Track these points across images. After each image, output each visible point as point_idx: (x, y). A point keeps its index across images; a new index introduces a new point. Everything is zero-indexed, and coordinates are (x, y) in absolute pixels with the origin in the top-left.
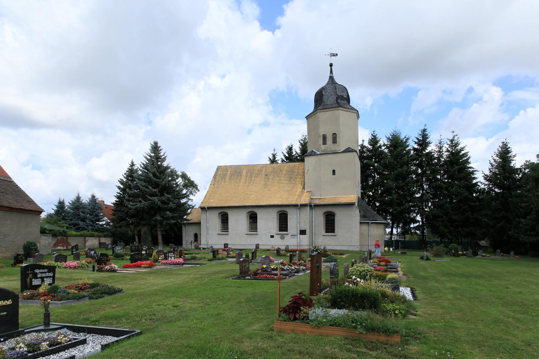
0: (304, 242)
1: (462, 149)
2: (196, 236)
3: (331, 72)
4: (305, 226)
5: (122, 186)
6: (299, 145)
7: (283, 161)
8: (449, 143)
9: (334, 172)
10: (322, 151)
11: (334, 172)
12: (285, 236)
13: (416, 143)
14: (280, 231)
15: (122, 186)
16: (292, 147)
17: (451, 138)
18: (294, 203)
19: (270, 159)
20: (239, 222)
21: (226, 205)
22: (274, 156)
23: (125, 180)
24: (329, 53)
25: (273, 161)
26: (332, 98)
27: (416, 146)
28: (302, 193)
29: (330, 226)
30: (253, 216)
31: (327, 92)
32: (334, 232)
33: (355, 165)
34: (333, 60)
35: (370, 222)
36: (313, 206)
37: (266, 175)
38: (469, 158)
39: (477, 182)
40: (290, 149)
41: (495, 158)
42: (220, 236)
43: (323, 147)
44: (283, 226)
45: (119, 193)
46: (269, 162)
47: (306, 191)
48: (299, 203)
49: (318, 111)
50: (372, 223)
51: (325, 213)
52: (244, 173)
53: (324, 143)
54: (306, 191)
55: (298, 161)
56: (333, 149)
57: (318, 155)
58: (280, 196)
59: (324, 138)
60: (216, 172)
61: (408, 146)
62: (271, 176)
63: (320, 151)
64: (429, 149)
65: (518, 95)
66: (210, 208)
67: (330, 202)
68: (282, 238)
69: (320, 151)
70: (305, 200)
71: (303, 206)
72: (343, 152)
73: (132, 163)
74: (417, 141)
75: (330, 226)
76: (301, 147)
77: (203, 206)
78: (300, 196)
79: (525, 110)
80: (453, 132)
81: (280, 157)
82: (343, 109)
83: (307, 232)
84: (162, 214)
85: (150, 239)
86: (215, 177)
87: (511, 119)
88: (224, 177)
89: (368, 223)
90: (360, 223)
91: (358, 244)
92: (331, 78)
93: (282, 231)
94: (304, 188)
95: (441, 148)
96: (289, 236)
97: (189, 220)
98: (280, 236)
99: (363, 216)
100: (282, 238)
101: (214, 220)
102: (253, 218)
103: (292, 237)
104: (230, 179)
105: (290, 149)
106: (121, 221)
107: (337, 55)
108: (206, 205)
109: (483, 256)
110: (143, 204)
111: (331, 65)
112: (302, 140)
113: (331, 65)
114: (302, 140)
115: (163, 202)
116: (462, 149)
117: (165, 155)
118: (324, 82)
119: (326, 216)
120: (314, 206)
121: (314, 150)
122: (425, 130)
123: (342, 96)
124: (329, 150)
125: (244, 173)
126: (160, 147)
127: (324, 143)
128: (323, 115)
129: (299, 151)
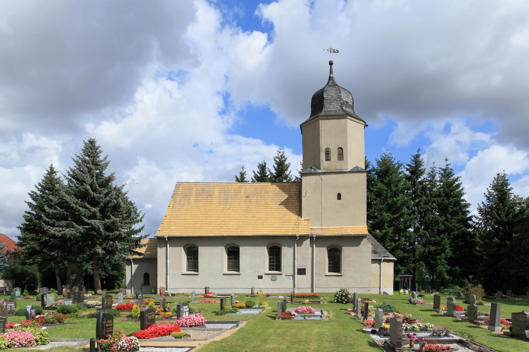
1: (457, 179)
3: (331, 72)
5: (34, 203)
6: (273, 163)
7: (253, 181)
9: (339, 197)
10: (324, 169)
11: (339, 197)
12: (277, 276)
13: (407, 170)
14: (270, 269)
15: (34, 203)
16: (265, 166)
18: (290, 233)
22: (242, 175)
23: (39, 193)
27: (407, 173)
29: (335, 265)
33: (357, 190)
34: (333, 57)
38: (462, 189)
39: (472, 216)
40: (263, 167)
41: (491, 191)
44: (275, 263)
45: (29, 213)
47: (303, 219)
48: (298, 234)
49: (320, 117)
53: (328, 159)
59: (328, 153)
60: (175, 190)
72: (351, 172)
73: (52, 168)
75: (335, 265)
76: (276, 166)
78: (297, 225)
81: (249, 176)
82: (350, 118)
90: (372, 260)
93: (273, 270)
95: (433, 177)
96: (284, 275)
99: (374, 252)
101: (178, 256)
102: (233, 254)
105: (263, 167)
106: (33, 255)
109: (502, 297)
110: (73, 231)
111: (331, 64)
112: (278, 158)
113: (331, 64)
114: (278, 158)
116: (457, 179)
117: (107, 160)
118: (322, 84)
120: (316, 237)
123: (347, 102)
124: (333, 170)
126: (98, 147)
127: (328, 159)
129: (274, 172)
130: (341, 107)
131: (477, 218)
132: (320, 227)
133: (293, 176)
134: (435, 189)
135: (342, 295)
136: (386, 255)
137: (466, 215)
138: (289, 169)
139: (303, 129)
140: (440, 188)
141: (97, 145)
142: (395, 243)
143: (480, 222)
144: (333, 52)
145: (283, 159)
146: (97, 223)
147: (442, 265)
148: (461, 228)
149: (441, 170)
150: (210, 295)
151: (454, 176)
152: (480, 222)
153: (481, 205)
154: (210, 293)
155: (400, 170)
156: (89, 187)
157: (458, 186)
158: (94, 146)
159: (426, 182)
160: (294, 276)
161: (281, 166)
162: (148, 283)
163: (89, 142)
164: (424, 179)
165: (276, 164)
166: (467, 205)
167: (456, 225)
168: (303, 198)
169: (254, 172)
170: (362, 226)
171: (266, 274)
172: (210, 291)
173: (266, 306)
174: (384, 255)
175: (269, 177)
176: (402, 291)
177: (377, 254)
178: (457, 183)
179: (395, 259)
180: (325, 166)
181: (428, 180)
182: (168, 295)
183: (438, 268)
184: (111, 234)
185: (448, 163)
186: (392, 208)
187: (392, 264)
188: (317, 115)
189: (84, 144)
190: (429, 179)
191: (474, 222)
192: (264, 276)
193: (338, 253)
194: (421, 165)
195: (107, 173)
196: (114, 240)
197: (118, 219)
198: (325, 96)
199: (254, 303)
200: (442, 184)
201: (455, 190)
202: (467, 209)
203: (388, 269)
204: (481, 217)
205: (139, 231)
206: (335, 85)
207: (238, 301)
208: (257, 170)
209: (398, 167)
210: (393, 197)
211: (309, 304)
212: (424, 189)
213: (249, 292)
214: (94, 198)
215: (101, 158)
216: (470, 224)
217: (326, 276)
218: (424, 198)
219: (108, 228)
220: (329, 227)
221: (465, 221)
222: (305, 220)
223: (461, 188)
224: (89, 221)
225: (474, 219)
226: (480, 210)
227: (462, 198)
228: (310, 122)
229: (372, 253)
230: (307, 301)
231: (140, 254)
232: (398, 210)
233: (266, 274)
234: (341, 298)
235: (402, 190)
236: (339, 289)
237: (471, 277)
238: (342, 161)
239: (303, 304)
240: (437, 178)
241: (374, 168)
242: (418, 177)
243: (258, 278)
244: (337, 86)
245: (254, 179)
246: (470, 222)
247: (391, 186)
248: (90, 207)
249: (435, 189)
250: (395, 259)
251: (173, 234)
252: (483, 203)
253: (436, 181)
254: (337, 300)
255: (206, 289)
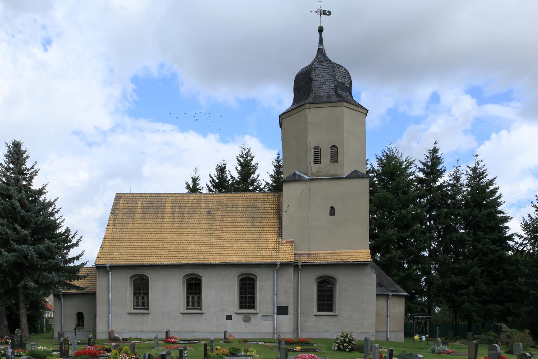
0: (285, 325)
1: (491, 183)
2: (80, 316)
3: (321, 42)
4: (288, 301)
6: (236, 163)
8: (471, 173)
9: (332, 211)
11: (332, 211)
12: (251, 316)
13: (420, 170)
14: (241, 308)
16: (225, 168)
17: (473, 165)
18: (268, 260)
19: (188, 186)
20: (167, 293)
21: (146, 262)
22: (194, 180)
24: (317, 8)
25: (194, 188)
26: (321, 86)
27: (421, 175)
28: (280, 244)
29: (326, 301)
30: (194, 282)
31: (319, 74)
32: (331, 310)
33: (357, 202)
34: (324, 21)
35: (391, 294)
36: (296, 267)
37: (209, 212)
38: (500, 197)
39: (512, 235)
40: (222, 170)
42: (133, 317)
43: (315, 168)
44: (248, 297)
46: (186, 191)
47: (284, 241)
48: (278, 261)
49: (307, 106)
50: (393, 295)
51: (132, 277)
52: (168, 208)
53: (317, 161)
54: (284, 241)
55: (237, 190)
56: (332, 172)
57: (306, 180)
58: (240, 247)
59: (317, 152)
61: (410, 174)
62: (218, 215)
63: (310, 174)
64: (440, 181)
65: (493, 110)
66: (115, 267)
67: (329, 260)
68: (247, 319)
69: (310, 174)
70: (286, 255)
71: (284, 265)
74: (422, 167)
75: (326, 301)
77: (100, 263)
78: (277, 249)
79: (497, 132)
80: (477, 156)
81: (204, 184)
82: (348, 105)
83: (291, 310)
84: (36, 277)
85: (6, 323)
86: (114, 211)
87: (478, 147)
88: (131, 213)
89: (388, 295)
90: (377, 295)
91: (374, 330)
92: (321, 51)
93: (246, 308)
94: (280, 234)
95: (458, 179)
96: (259, 316)
97: (83, 289)
98: (242, 316)
99: (379, 285)
100: (247, 319)
101: (122, 289)
102: (194, 287)
103: (264, 318)
104: (143, 217)
105: (222, 170)
107: (330, 13)
108: (107, 262)
111: (321, 30)
112: (242, 157)
113: (321, 30)
114: (242, 157)
115: (41, 255)
116: (491, 183)
117: (36, 168)
118: (308, 58)
119: (241, 280)
120: (302, 266)
121: (298, 173)
122: (435, 151)
123: (343, 84)
125: (168, 208)
127: (317, 161)
128: (315, 115)
129: (236, 175)
130: (336, 91)
131: (520, 237)
132: (307, 252)
133: (262, 181)
134: (459, 197)
135: (345, 341)
136: (395, 290)
137: (506, 232)
138: (257, 172)
139: (284, 121)
140: (468, 194)
141: (23, 149)
142: (404, 272)
143: (525, 242)
144: (324, 14)
145: (249, 158)
146: (31, 250)
147: (471, 302)
148: (497, 251)
149: (468, 169)
150: (173, 340)
151: (487, 178)
152: (525, 242)
153: (527, 219)
154: (171, 338)
155: (410, 171)
156: (17, 204)
157: (494, 192)
158: (19, 150)
159: (446, 186)
160: (272, 316)
161: (247, 167)
162: (83, 325)
163: (13, 144)
164: (444, 182)
165: (239, 165)
166: (507, 219)
167: (491, 247)
168: (284, 214)
169: (211, 176)
170: (363, 251)
171: (237, 313)
172: (171, 336)
173: (253, 353)
174: (392, 289)
175: (230, 182)
176: (417, 337)
177: (383, 288)
178: (492, 187)
179: (406, 294)
180: (314, 171)
181: (449, 185)
182: (119, 340)
183: (463, 306)
184: (45, 263)
185: (479, 159)
186: (404, 224)
187: (403, 301)
188: (302, 103)
189: (7, 148)
190: (451, 182)
191: (517, 243)
192: (235, 317)
193: (331, 286)
194: (440, 163)
195: (36, 185)
196: (50, 271)
197: (54, 244)
198: (314, 77)
199: (239, 350)
200: (469, 189)
201: (489, 198)
202: (506, 225)
203: (397, 309)
204: (526, 236)
205: (77, 258)
206: (327, 60)
207: (219, 348)
208: (214, 173)
209: (407, 167)
210: (401, 209)
211: (301, 351)
212: (445, 196)
213: (222, 336)
214: (23, 218)
215: (28, 164)
216: (509, 245)
217: (315, 316)
218: (445, 210)
219: (41, 255)
220: (318, 252)
221: (502, 239)
222: (287, 242)
223: (497, 194)
224: (20, 247)
225: (516, 239)
226: (526, 226)
227: (499, 208)
228: (294, 112)
229: (377, 287)
230: (298, 348)
231: (77, 288)
232: (408, 227)
233: (237, 313)
234: (343, 345)
235: (413, 199)
236: (340, 334)
237: (510, 319)
238: (336, 164)
239: (293, 351)
240: (464, 180)
241: (373, 168)
242: (435, 180)
243: (227, 319)
244: (330, 61)
245: (210, 184)
246: (511, 243)
247: (397, 194)
248: (21, 230)
249: (459, 197)
250: (406, 294)
251: (116, 262)
252: (529, 216)
253: (462, 185)
254: (338, 347)
255: (167, 332)
